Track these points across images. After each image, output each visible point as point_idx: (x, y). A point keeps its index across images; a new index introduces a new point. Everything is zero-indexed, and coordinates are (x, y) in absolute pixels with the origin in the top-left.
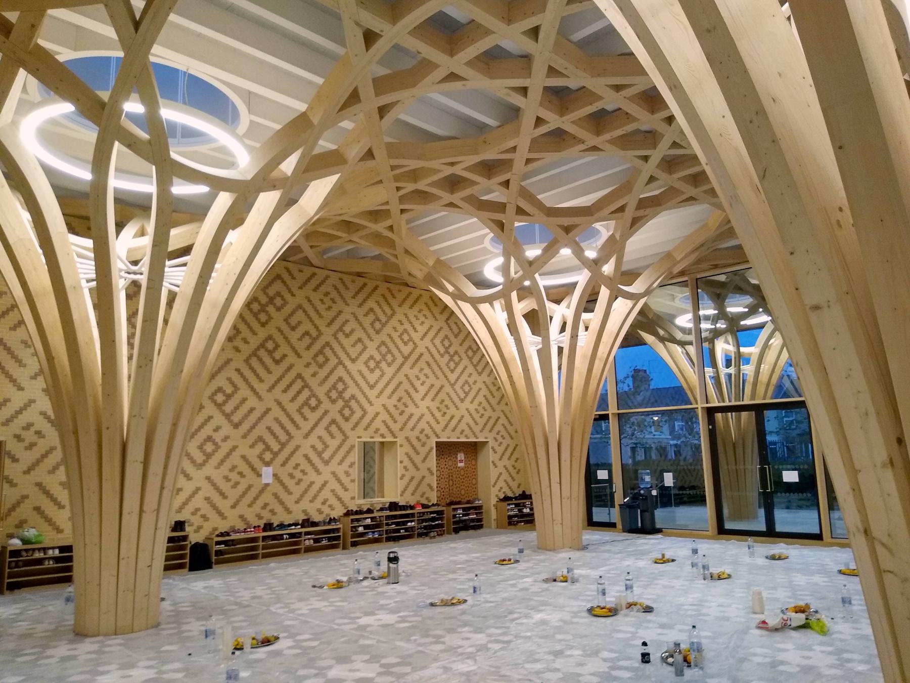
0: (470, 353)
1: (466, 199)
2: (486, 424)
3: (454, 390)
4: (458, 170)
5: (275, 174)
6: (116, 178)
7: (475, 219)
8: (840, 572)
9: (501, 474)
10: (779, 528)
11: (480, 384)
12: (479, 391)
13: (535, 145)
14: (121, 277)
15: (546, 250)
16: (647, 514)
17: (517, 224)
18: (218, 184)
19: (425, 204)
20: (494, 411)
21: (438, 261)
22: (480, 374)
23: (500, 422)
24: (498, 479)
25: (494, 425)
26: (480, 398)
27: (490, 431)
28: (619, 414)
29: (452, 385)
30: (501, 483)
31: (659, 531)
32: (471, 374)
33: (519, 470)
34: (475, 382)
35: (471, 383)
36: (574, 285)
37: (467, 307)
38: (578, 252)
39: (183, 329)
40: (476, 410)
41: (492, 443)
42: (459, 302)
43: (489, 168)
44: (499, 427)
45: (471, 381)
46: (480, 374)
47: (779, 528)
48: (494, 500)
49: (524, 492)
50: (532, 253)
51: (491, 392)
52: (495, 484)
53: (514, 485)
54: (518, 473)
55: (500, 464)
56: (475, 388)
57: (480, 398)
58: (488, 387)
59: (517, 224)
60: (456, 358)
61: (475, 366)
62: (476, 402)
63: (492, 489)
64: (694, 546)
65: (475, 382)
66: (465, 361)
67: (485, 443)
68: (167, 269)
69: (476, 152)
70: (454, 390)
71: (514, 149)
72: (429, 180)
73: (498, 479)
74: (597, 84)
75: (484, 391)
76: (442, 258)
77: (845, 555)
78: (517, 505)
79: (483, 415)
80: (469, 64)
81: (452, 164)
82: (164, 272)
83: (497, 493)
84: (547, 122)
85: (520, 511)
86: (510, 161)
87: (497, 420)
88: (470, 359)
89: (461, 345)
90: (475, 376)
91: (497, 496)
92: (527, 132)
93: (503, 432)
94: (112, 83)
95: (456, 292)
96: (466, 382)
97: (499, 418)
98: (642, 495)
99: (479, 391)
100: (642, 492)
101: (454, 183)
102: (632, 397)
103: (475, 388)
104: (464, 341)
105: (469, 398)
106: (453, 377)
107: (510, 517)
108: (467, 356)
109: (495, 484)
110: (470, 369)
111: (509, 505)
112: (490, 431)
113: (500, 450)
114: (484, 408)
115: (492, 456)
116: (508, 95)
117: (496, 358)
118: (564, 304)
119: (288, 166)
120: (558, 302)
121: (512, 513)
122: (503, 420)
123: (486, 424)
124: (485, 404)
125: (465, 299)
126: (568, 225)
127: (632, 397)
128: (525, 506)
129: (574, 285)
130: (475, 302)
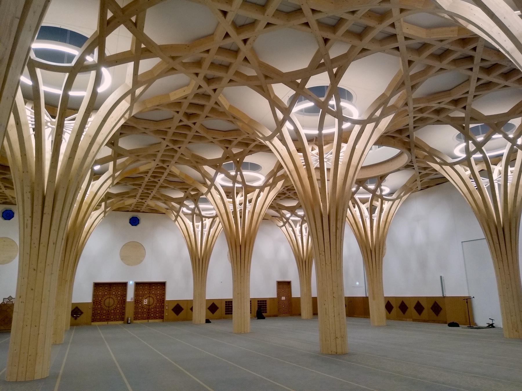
4: (442, 106)
5: (374, 117)
6: (44, 85)
13: (478, 88)
14: (49, 127)
17: (471, 126)
18: (355, 122)
36: (502, 155)
37: (448, 168)
38: (506, 137)
39: (87, 150)
42: (444, 166)
43: (456, 102)
59: (471, 126)
68: (66, 122)
71: (467, 92)
72: (428, 112)
80: (449, 63)
81: (439, 103)
82: (64, 124)
84: (435, 67)
86: (466, 98)
92: (474, 84)
94: (326, 96)
101: (438, 112)
102: (219, 214)
117: (463, 194)
118: (499, 165)
119: (378, 114)
120: (496, 165)
125: (446, 164)
126: (497, 124)
127: (219, 214)
129: (502, 155)
130: (452, 165)
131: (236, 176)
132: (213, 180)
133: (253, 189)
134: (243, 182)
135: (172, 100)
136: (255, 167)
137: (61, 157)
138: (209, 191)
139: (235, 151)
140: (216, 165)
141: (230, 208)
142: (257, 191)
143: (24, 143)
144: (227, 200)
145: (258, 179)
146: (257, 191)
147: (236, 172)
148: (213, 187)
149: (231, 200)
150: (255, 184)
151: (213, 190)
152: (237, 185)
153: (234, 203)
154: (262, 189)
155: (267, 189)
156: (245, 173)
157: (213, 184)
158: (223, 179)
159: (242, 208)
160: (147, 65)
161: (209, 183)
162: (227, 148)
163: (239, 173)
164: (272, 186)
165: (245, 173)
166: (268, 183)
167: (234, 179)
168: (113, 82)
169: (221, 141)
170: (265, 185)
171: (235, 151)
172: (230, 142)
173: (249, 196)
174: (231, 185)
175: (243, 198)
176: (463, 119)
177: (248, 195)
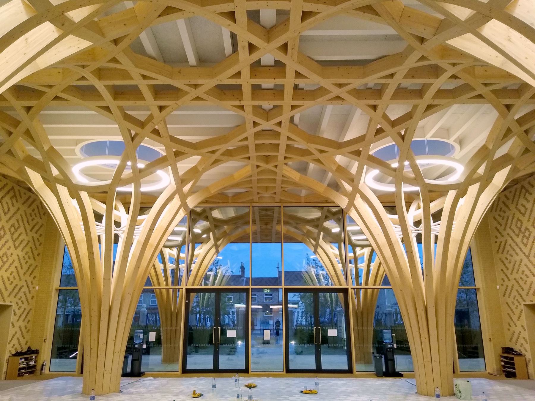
0: (13, 230)
1: (121, 108)
2: (13, 290)
3: (529, 260)
7: (117, 126)
8: (302, 392)
9: (16, 333)
10: (324, 367)
11: (15, 257)
12: (13, 263)
15: (148, 167)
16: (136, 363)
19: (82, 99)
20: (20, 280)
21: (52, 149)
22: (16, 248)
23: (23, 290)
24: (13, 337)
25: (19, 291)
26: (13, 269)
27: (15, 297)
28: (60, 290)
29: (528, 257)
30: (15, 341)
31: (399, 375)
32: (10, 247)
33: (29, 330)
34: (12, 254)
35: (9, 255)
40: (8, 278)
41: (14, 307)
44: (21, 294)
45: (9, 253)
46: (16, 248)
47: (324, 367)
48: (7, 355)
49: (29, 348)
50: (141, 165)
51: (21, 264)
52: (10, 341)
53: (23, 342)
54: (27, 332)
55: (17, 325)
56: (11, 260)
57: (13, 269)
58: (19, 260)
60: (527, 234)
61: (14, 241)
62: (10, 271)
63: (8, 346)
64: (214, 382)
65: (12, 254)
66: (8, 236)
67: (10, 306)
69: (170, 75)
70: (529, 260)
73: (13, 337)
74: (135, 72)
75: (17, 263)
76: (55, 147)
77: (389, 382)
78: (26, 359)
79: (12, 282)
83: (11, 349)
85: (27, 364)
87: (21, 288)
88: (12, 234)
89: (7, 222)
90: (12, 250)
91: (10, 352)
93: (24, 299)
95: (61, 177)
96: (5, 253)
97: (22, 286)
98: (136, 349)
99: (13, 263)
100: (136, 346)
103: (11, 260)
104: (10, 219)
105: (6, 267)
106: (526, 251)
107: (20, 369)
108: (10, 231)
109: (10, 341)
110: (10, 243)
111: (21, 359)
112: (15, 297)
113: (18, 312)
114: (14, 277)
115: (13, 318)
116: (244, 48)
121: (22, 366)
122: (25, 289)
123: (13, 290)
124: (15, 274)
128: (31, 360)
131: (402, 167)
132: (353, 180)
133: (439, 192)
134: (418, 179)
135: (212, 192)
136: (439, 148)
137: (333, 299)
138: (352, 204)
139: (396, 111)
140: (356, 149)
141: (396, 234)
142: (452, 194)
143: (88, 219)
144: (388, 218)
145: (449, 171)
146: (452, 194)
147: (401, 162)
148: (358, 196)
149: (396, 217)
150: (452, 179)
151: (358, 201)
152: (406, 188)
153: (402, 223)
154: (461, 190)
155: (473, 189)
156: (420, 161)
157: (356, 190)
158: (379, 179)
159: (422, 232)
160: (185, 165)
161: (348, 188)
162: (374, 107)
163: (407, 163)
164: (485, 181)
165: (420, 161)
166: (475, 176)
167: (398, 177)
168: (163, 180)
169: (358, 93)
170: (469, 181)
171: (396, 111)
172: (378, 92)
173: (434, 207)
174: (391, 189)
175: (421, 211)
176: (318, 219)
177: (432, 205)
